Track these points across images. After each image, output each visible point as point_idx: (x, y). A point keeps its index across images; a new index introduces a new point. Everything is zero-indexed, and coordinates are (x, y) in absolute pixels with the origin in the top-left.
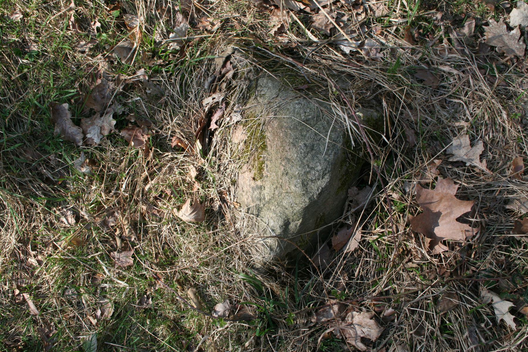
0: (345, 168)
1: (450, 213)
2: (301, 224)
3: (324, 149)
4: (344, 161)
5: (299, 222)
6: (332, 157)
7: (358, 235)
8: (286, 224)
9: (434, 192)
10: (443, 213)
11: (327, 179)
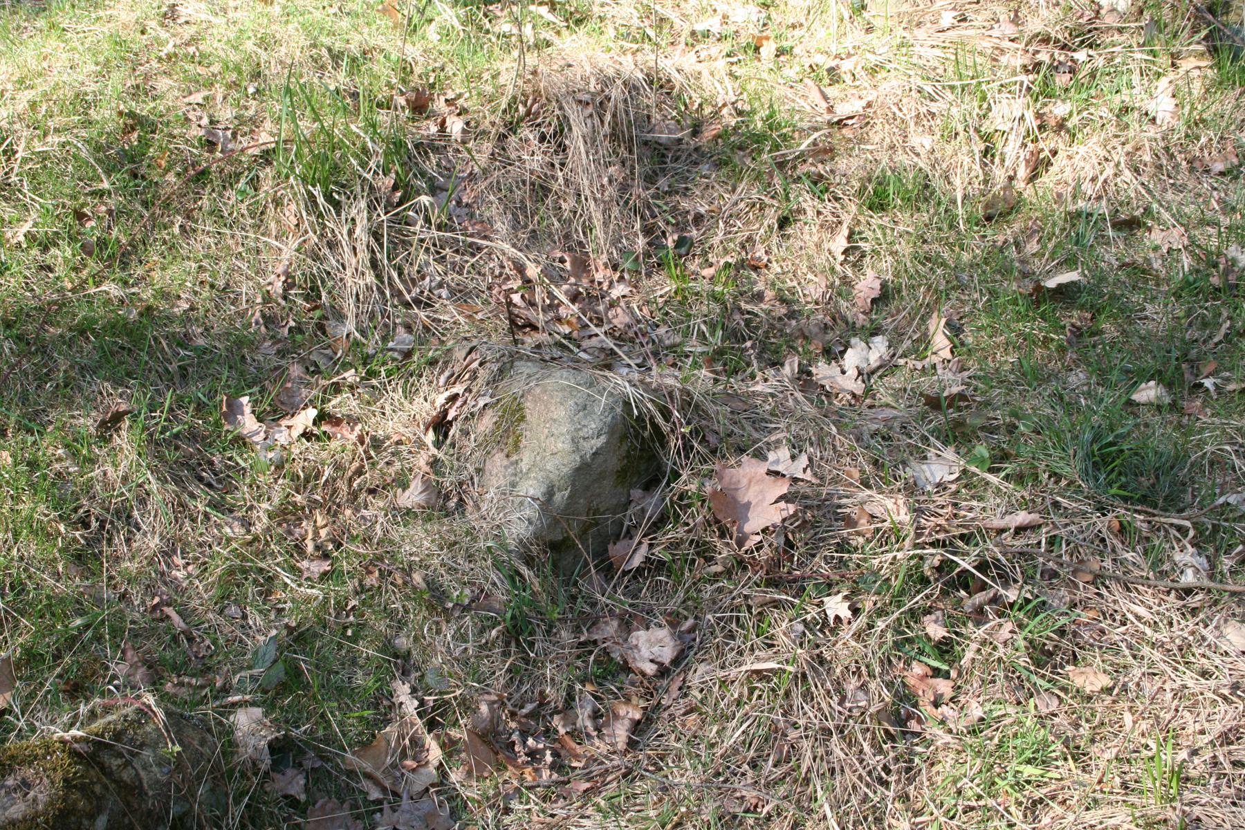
0: (624, 448)
1: (762, 501)
2: (569, 497)
3: (599, 410)
4: (624, 438)
5: (567, 493)
6: (609, 418)
7: (644, 550)
8: (550, 493)
9: (741, 470)
10: (754, 503)
11: (603, 439)
